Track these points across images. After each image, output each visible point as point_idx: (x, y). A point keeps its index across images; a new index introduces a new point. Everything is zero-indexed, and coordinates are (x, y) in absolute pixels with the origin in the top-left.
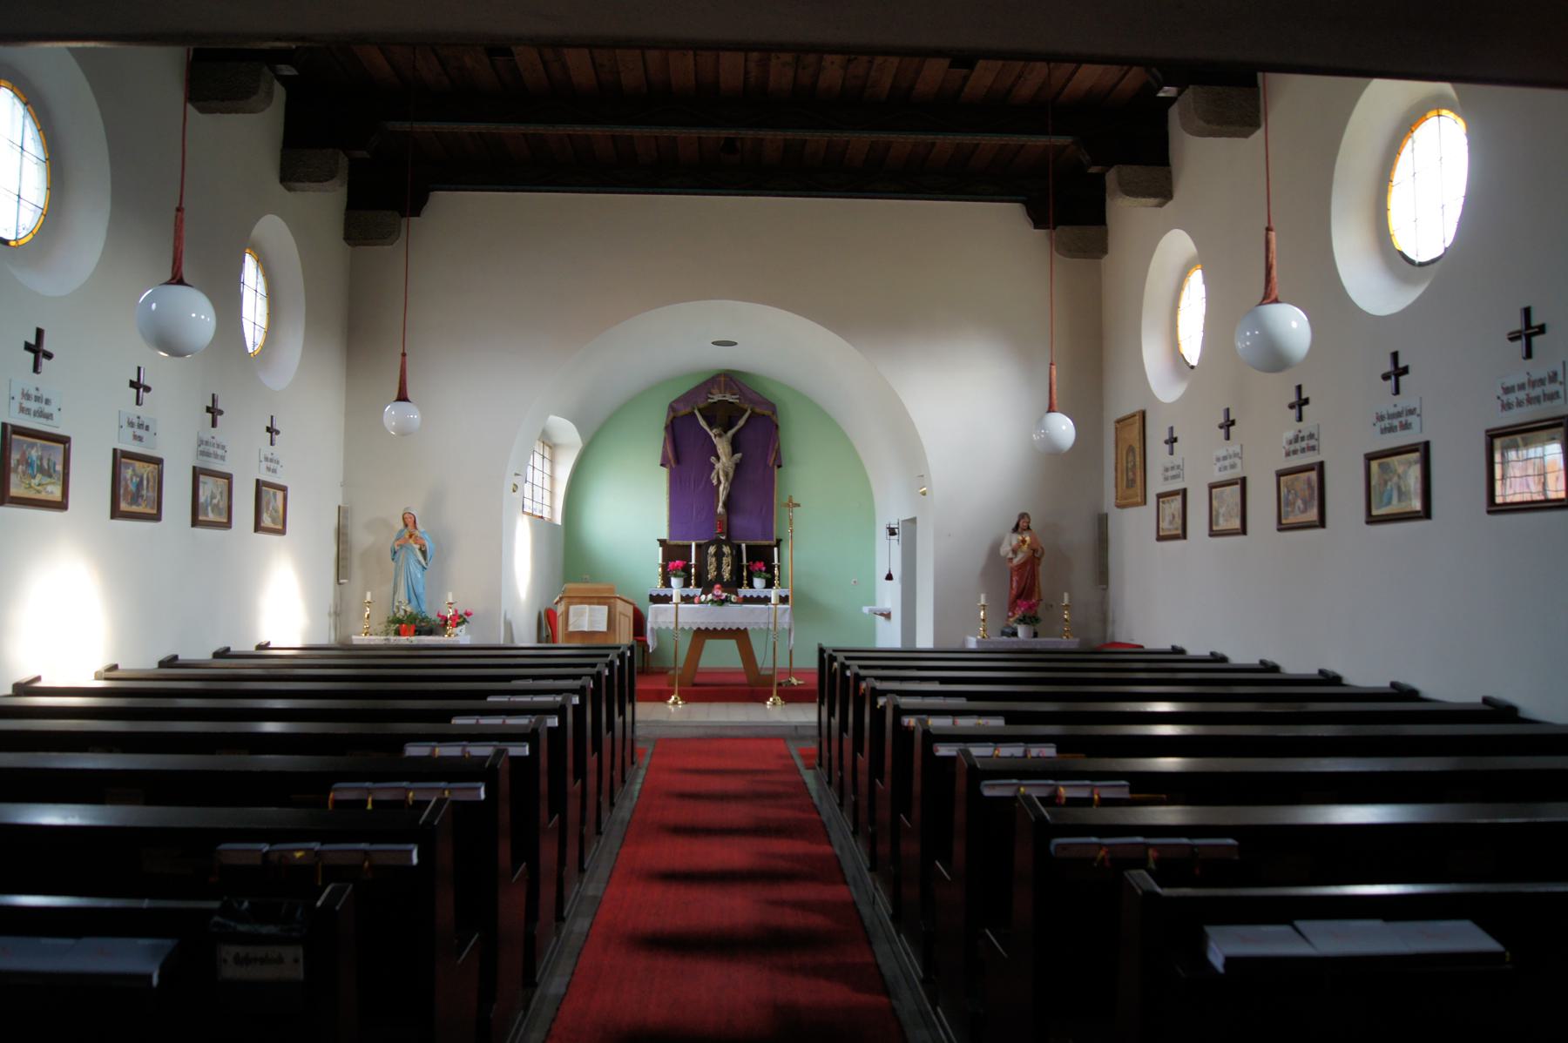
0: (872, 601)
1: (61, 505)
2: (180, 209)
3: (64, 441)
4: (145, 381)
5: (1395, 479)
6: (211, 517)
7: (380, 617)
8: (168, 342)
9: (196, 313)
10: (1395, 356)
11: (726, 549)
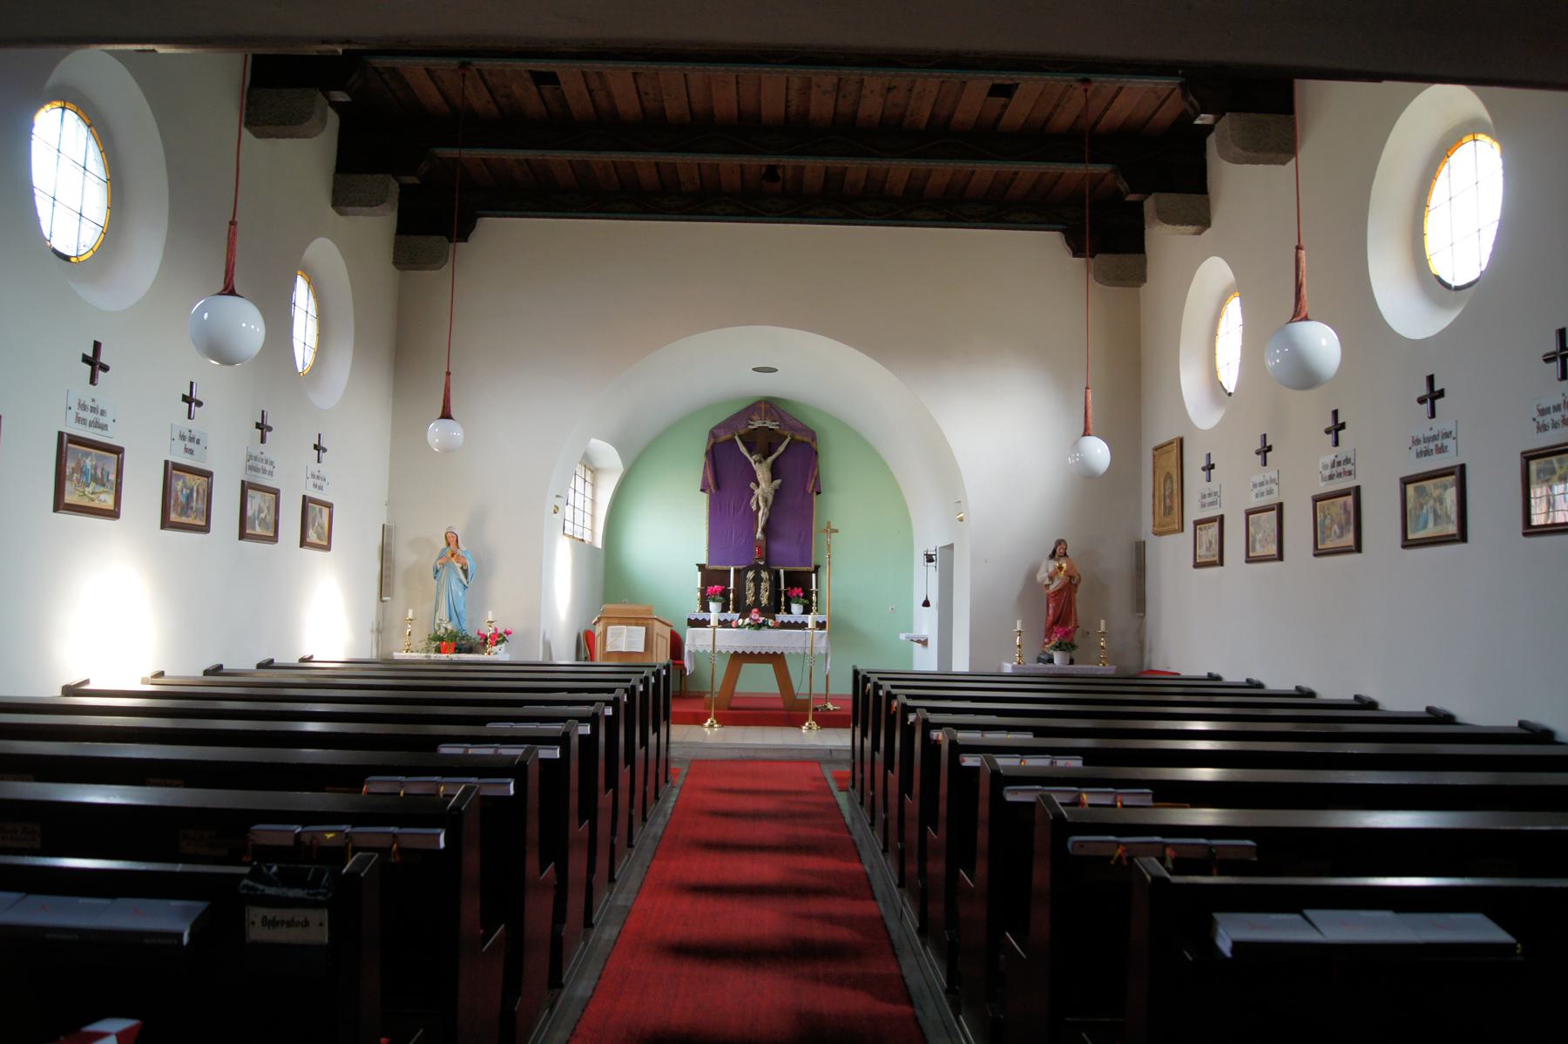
0: (910, 628)
1: (113, 514)
2: (233, 223)
3: (118, 451)
4: (197, 395)
5: (1431, 502)
6: (259, 531)
7: (420, 636)
8: (218, 350)
9: (245, 323)
10: (1431, 379)
11: (764, 575)
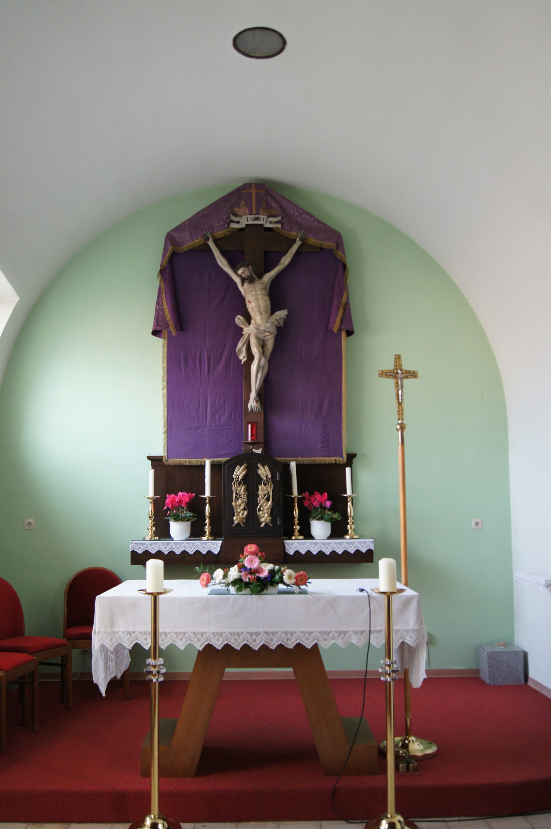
11: (264, 472)
